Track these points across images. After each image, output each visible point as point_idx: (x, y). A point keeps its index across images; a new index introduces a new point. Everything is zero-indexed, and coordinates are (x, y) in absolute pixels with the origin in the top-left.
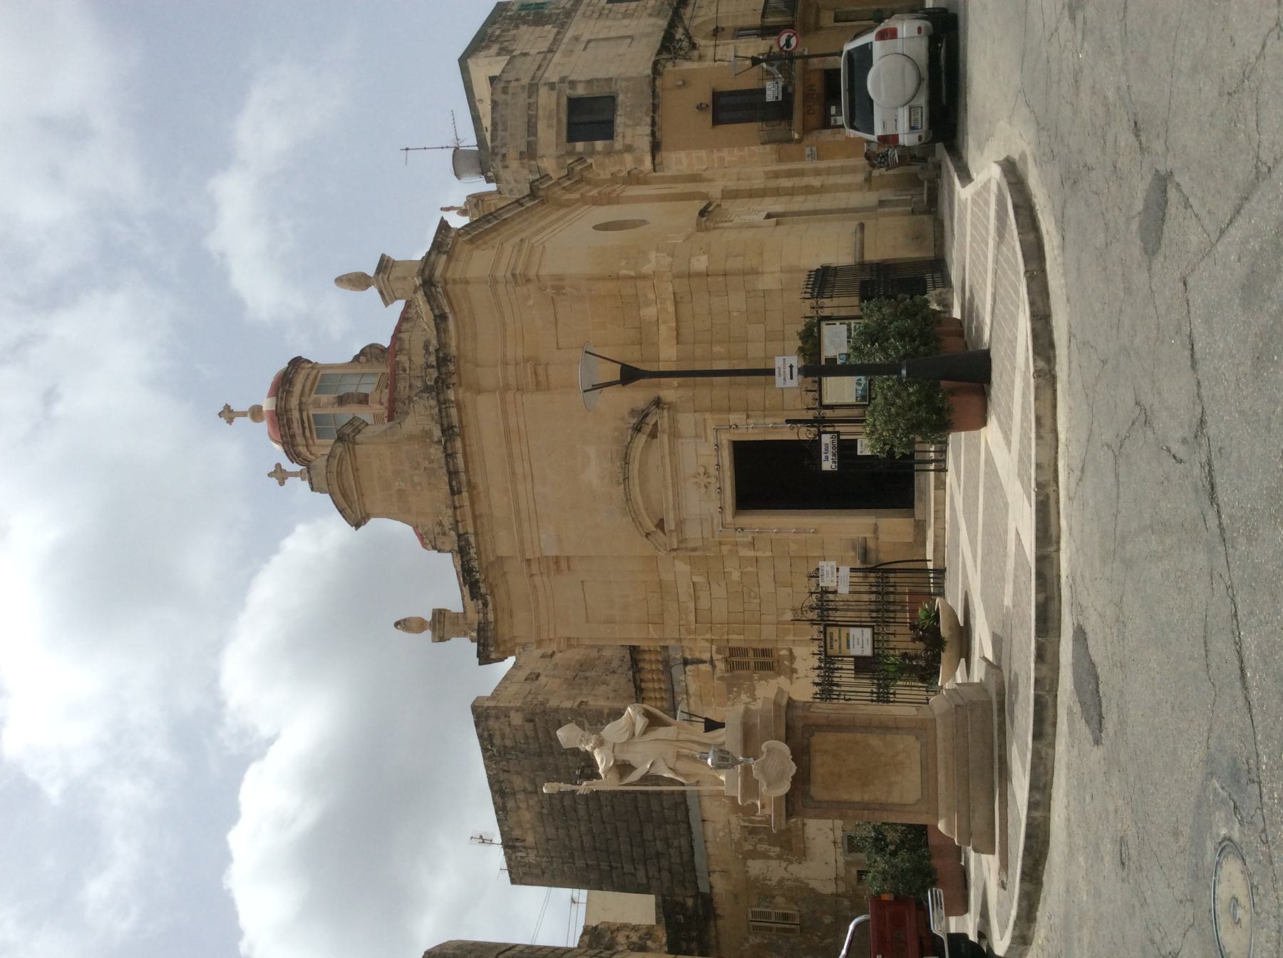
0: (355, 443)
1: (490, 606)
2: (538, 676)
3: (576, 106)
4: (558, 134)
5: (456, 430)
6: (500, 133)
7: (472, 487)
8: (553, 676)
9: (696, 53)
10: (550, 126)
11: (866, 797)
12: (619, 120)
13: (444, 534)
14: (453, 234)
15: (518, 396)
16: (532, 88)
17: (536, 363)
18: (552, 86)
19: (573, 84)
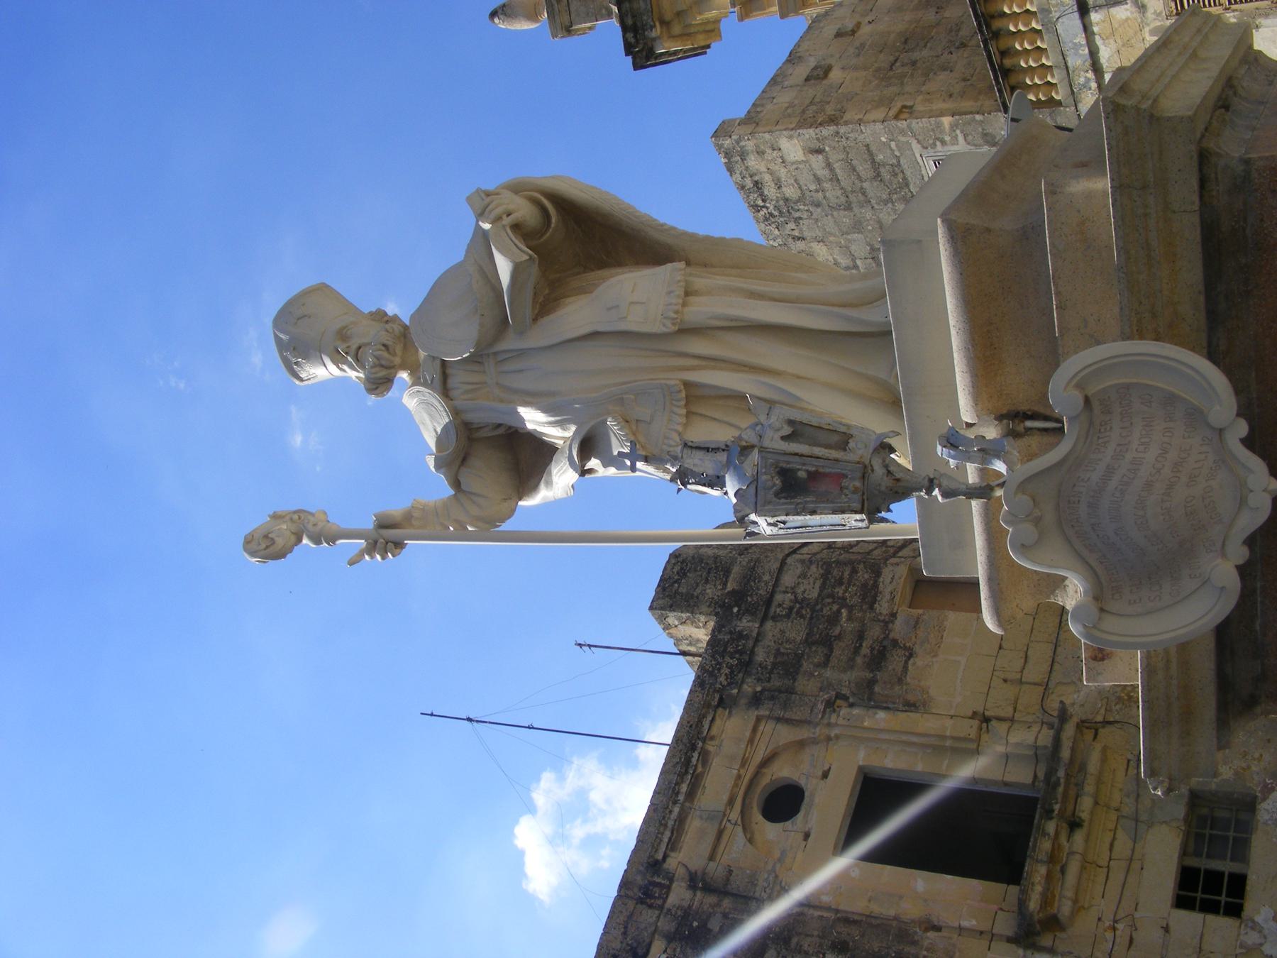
2: (827, 70)
8: (856, 68)
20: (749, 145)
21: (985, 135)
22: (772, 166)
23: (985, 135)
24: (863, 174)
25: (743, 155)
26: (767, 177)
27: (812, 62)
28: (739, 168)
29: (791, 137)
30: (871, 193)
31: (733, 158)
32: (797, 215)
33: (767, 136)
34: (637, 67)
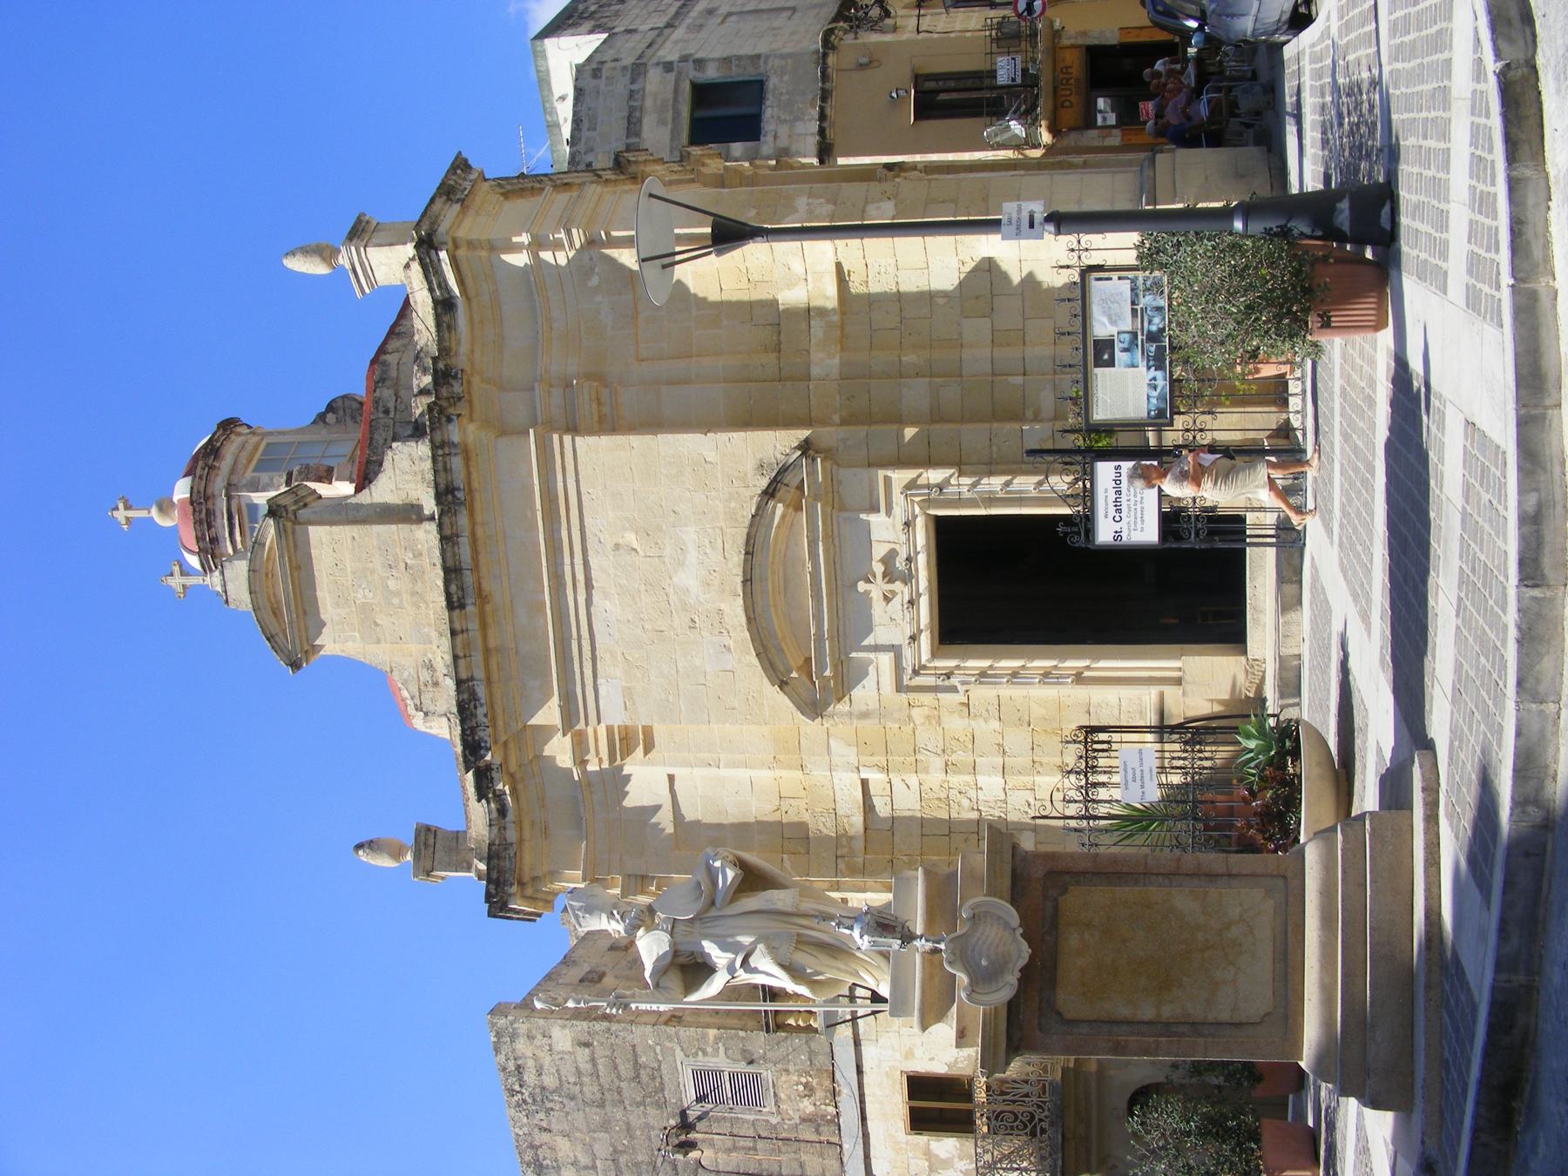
0: (296, 521)
1: (511, 816)
2: (602, 976)
3: (703, 94)
4: (674, 134)
5: (460, 495)
6: (585, 134)
7: (483, 598)
9: (888, 21)
10: (662, 122)
11: (1167, 1012)
12: (769, 112)
13: (436, 684)
14: (473, 176)
15: (567, 439)
16: (638, 70)
17: (601, 379)
18: (668, 67)
19: (700, 63)
20: (522, 1028)
21: (744, 1051)
22: (538, 1052)
23: (744, 1051)
24: (623, 1073)
25: (513, 1037)
26: (531, 1063)
27: (586, 968)
28: (505, 1049)
29: (564, 1027)
30: (626, 1094)
31: (503, 1037)
32: (549, 1105)
33: (541, 1022)
34: (491, 914)
